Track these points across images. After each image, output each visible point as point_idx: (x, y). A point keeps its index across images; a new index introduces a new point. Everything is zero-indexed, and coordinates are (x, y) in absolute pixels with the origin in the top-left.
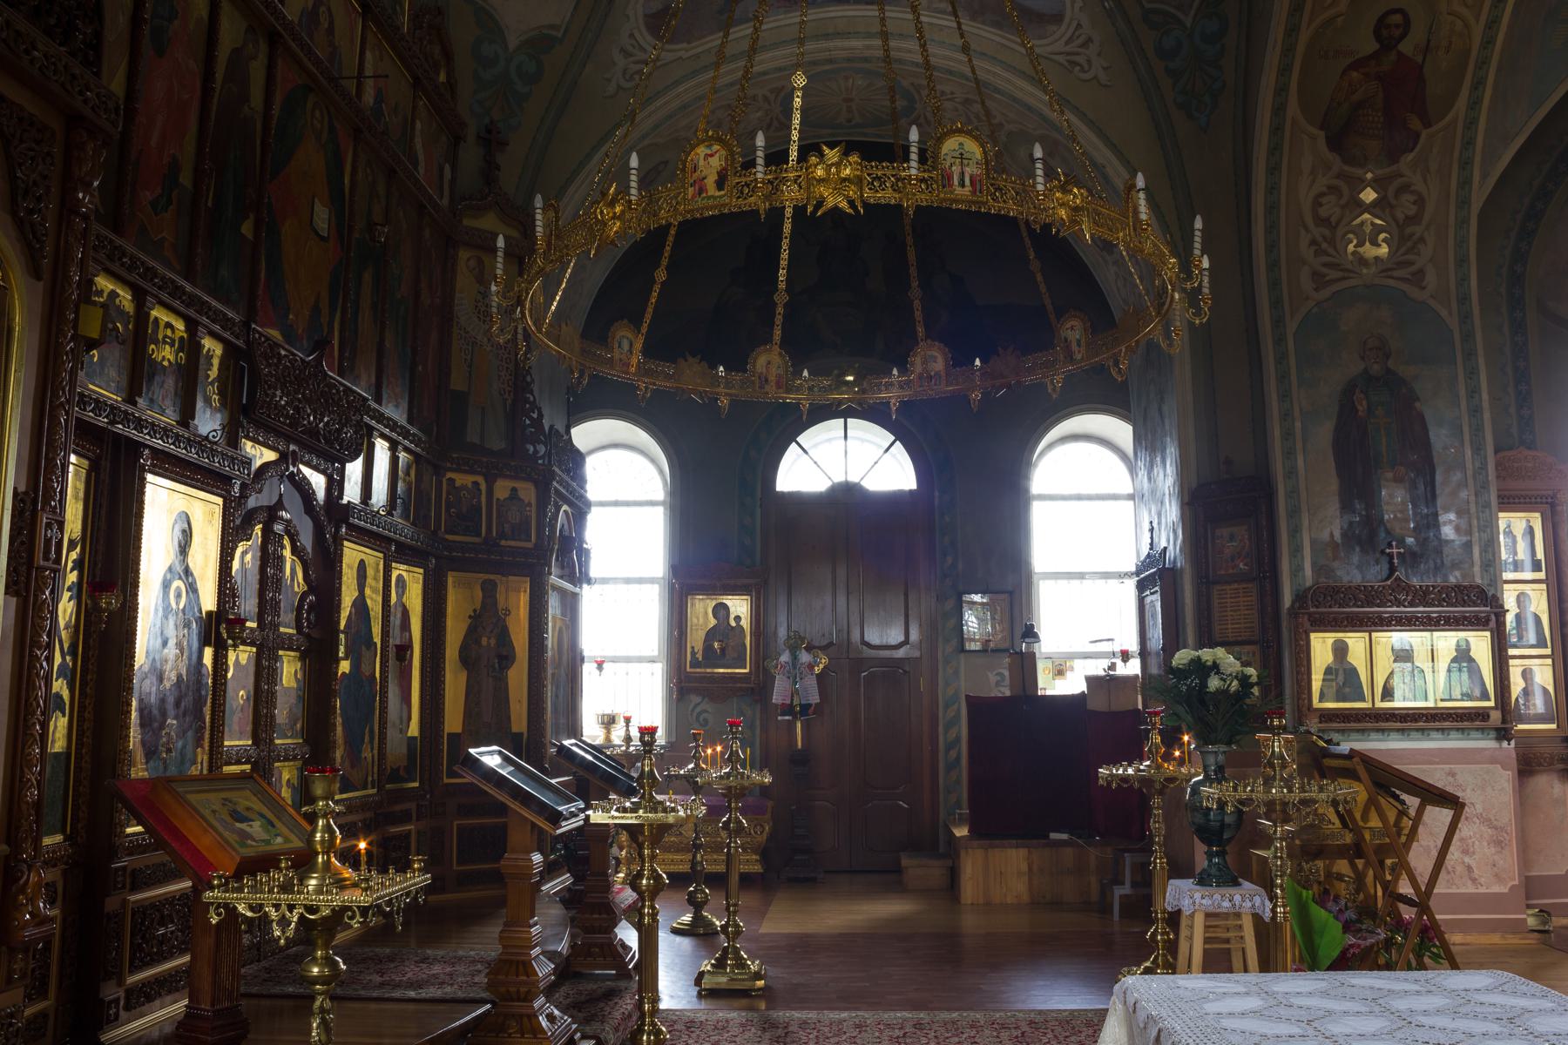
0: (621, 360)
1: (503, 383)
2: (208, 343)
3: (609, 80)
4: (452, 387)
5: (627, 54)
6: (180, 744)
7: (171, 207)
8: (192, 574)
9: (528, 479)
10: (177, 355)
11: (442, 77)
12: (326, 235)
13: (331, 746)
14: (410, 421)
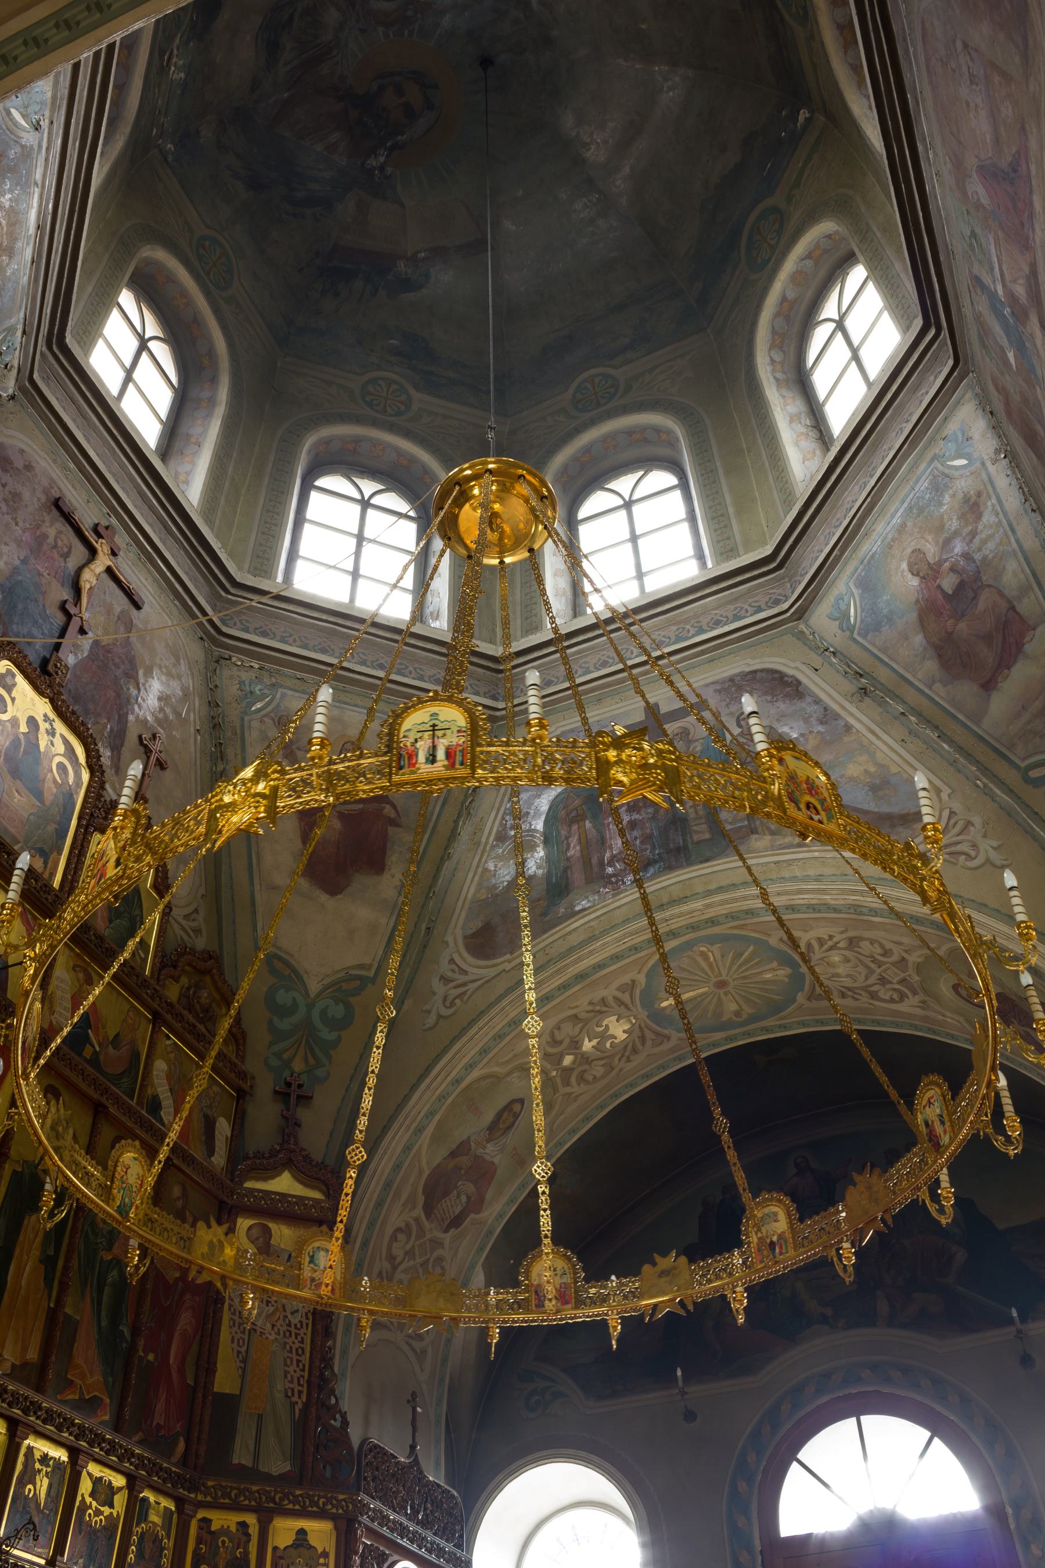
1: (291, 1382)
3: (429, 1012)
5: (445, 980)
9: (321, 1515)
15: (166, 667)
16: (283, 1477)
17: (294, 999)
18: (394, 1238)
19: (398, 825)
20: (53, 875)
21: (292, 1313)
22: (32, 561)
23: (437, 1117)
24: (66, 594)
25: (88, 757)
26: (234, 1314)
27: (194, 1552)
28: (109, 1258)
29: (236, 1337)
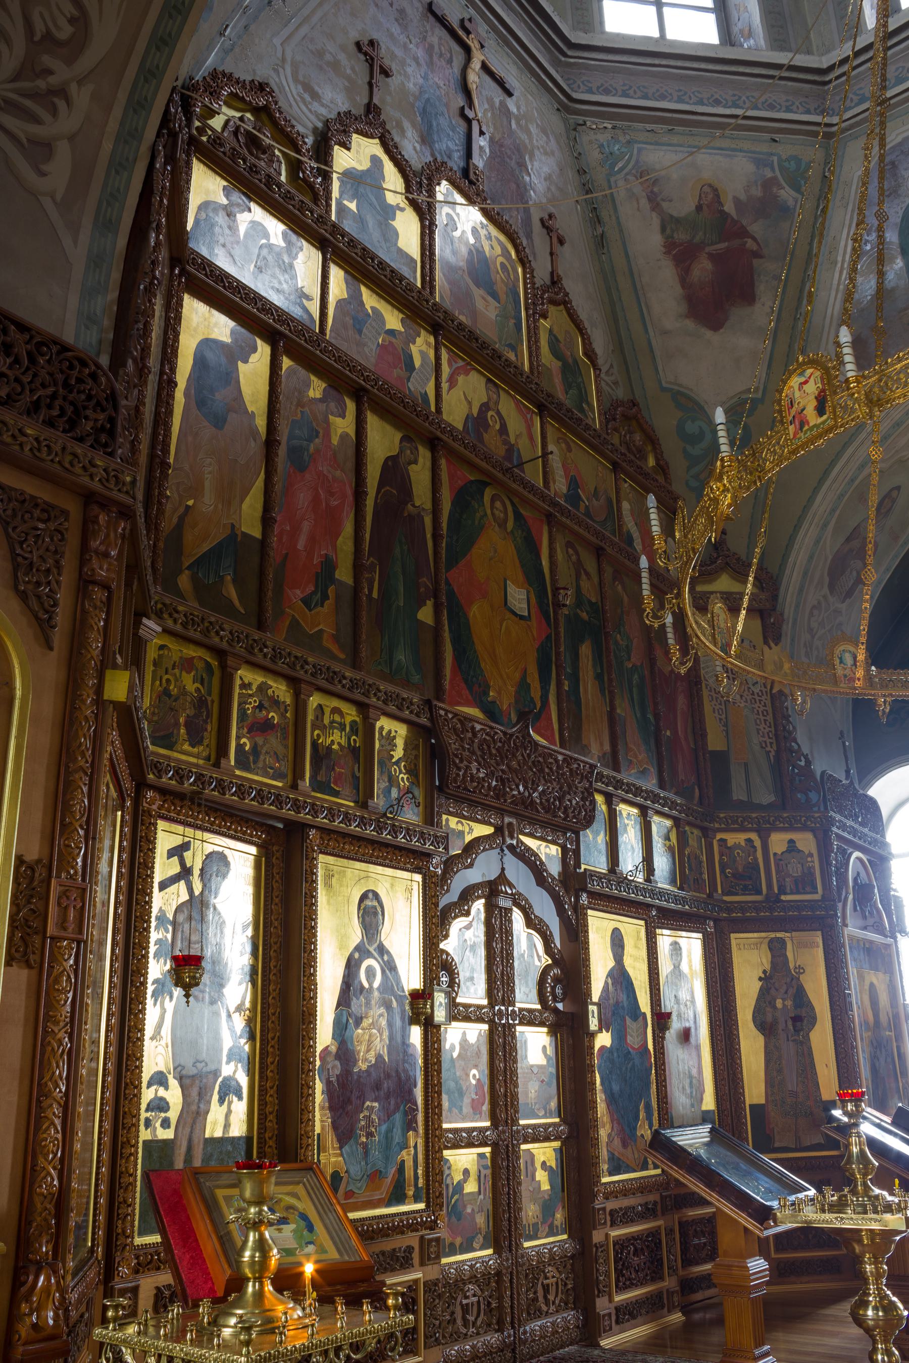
0: (845, 676)
1: (763, 737)
2: (384, 724)
4: (710, 748)
6: (384, 1128)
7: (327, 602)
8: (388, 953)
9: (804, 828)
10: (349, 739)
11: (651, 462)
12: (526, 614)
13: (594, 1125)
14: (662, 785)
15: (542, 147)
16: (770, 806)
17: (700, 427)
18: (811, 614)
19: (761, 257)
20: (523, 364)
21: (754, 685)
22: (431, 76)
23: (838, 512)
24: (461, 101)
25: (517, 252)
26: (710, 691)
28: (631, 666)
29: (717, 708)
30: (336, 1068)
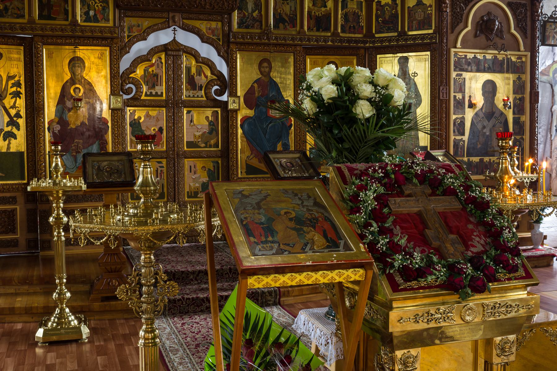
27: (376, 15)
30: (57, 128)
